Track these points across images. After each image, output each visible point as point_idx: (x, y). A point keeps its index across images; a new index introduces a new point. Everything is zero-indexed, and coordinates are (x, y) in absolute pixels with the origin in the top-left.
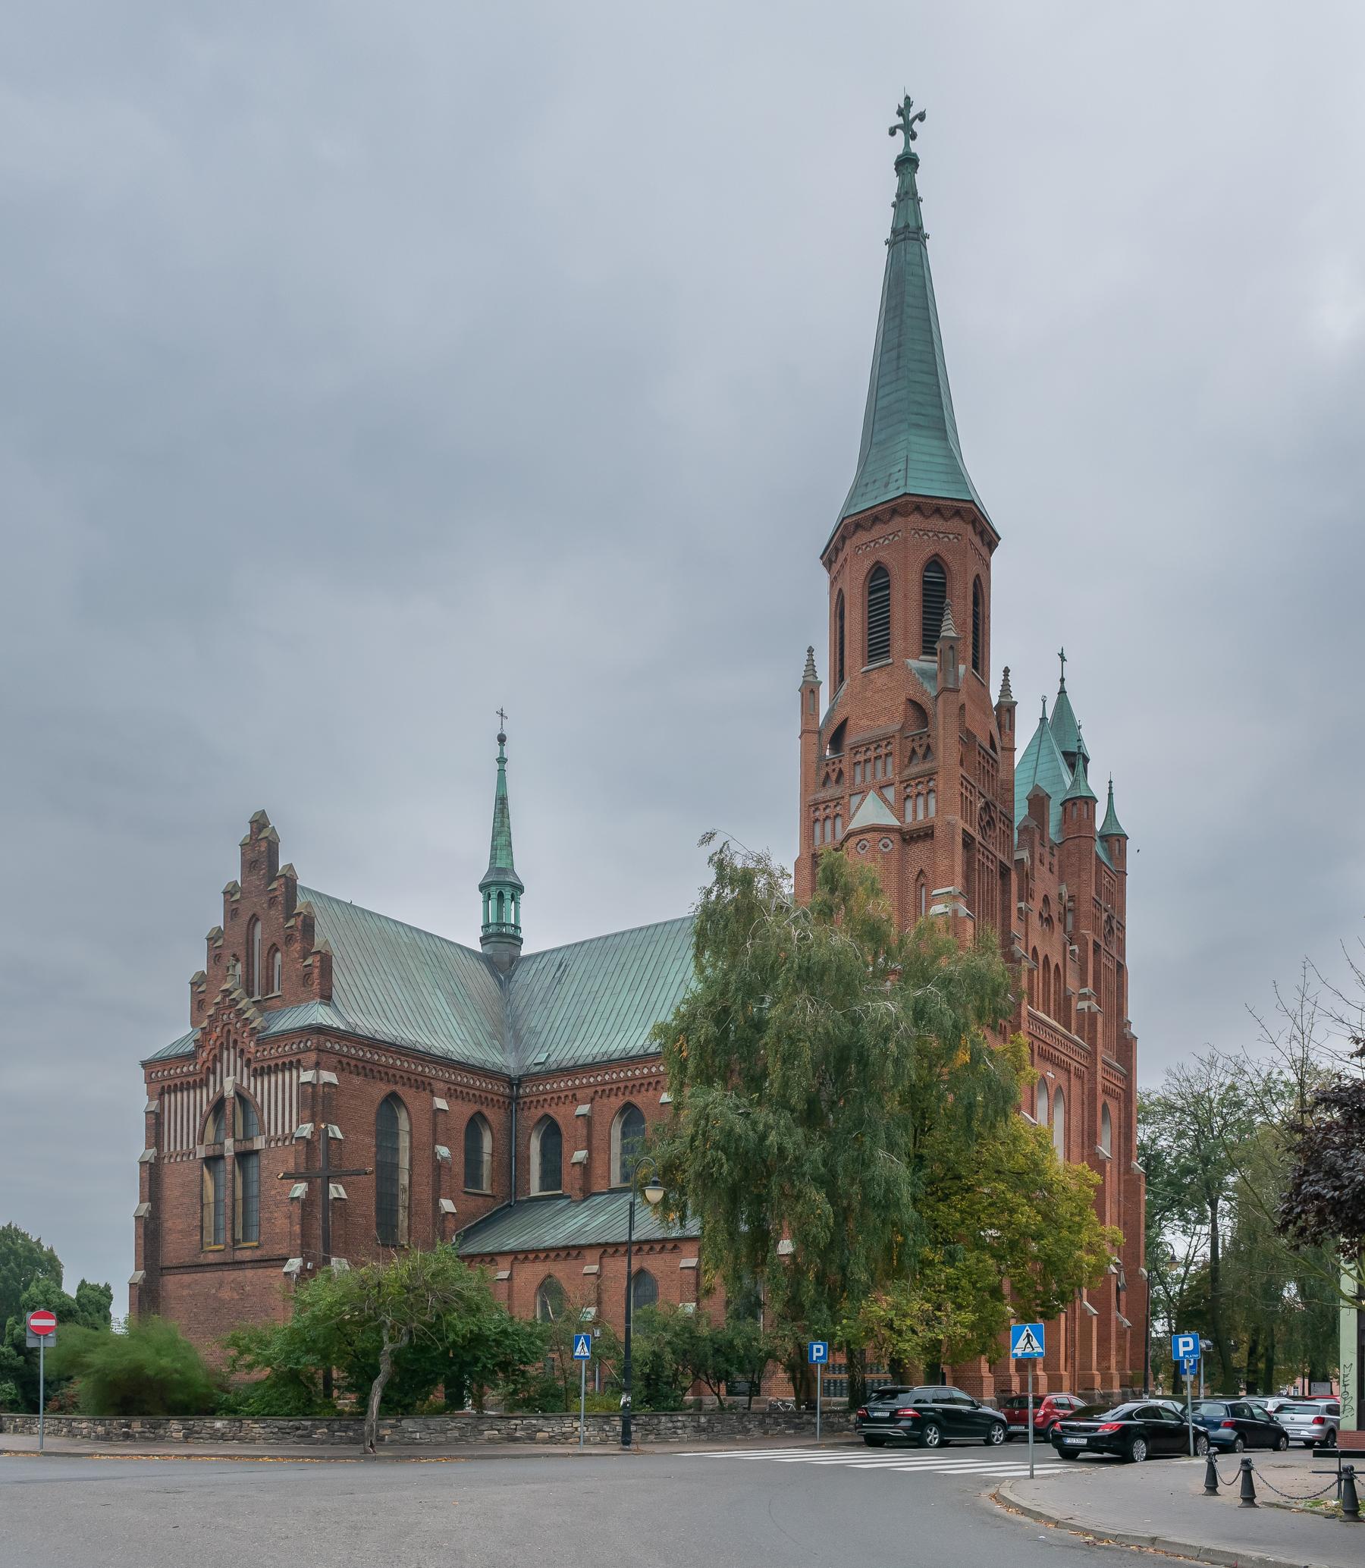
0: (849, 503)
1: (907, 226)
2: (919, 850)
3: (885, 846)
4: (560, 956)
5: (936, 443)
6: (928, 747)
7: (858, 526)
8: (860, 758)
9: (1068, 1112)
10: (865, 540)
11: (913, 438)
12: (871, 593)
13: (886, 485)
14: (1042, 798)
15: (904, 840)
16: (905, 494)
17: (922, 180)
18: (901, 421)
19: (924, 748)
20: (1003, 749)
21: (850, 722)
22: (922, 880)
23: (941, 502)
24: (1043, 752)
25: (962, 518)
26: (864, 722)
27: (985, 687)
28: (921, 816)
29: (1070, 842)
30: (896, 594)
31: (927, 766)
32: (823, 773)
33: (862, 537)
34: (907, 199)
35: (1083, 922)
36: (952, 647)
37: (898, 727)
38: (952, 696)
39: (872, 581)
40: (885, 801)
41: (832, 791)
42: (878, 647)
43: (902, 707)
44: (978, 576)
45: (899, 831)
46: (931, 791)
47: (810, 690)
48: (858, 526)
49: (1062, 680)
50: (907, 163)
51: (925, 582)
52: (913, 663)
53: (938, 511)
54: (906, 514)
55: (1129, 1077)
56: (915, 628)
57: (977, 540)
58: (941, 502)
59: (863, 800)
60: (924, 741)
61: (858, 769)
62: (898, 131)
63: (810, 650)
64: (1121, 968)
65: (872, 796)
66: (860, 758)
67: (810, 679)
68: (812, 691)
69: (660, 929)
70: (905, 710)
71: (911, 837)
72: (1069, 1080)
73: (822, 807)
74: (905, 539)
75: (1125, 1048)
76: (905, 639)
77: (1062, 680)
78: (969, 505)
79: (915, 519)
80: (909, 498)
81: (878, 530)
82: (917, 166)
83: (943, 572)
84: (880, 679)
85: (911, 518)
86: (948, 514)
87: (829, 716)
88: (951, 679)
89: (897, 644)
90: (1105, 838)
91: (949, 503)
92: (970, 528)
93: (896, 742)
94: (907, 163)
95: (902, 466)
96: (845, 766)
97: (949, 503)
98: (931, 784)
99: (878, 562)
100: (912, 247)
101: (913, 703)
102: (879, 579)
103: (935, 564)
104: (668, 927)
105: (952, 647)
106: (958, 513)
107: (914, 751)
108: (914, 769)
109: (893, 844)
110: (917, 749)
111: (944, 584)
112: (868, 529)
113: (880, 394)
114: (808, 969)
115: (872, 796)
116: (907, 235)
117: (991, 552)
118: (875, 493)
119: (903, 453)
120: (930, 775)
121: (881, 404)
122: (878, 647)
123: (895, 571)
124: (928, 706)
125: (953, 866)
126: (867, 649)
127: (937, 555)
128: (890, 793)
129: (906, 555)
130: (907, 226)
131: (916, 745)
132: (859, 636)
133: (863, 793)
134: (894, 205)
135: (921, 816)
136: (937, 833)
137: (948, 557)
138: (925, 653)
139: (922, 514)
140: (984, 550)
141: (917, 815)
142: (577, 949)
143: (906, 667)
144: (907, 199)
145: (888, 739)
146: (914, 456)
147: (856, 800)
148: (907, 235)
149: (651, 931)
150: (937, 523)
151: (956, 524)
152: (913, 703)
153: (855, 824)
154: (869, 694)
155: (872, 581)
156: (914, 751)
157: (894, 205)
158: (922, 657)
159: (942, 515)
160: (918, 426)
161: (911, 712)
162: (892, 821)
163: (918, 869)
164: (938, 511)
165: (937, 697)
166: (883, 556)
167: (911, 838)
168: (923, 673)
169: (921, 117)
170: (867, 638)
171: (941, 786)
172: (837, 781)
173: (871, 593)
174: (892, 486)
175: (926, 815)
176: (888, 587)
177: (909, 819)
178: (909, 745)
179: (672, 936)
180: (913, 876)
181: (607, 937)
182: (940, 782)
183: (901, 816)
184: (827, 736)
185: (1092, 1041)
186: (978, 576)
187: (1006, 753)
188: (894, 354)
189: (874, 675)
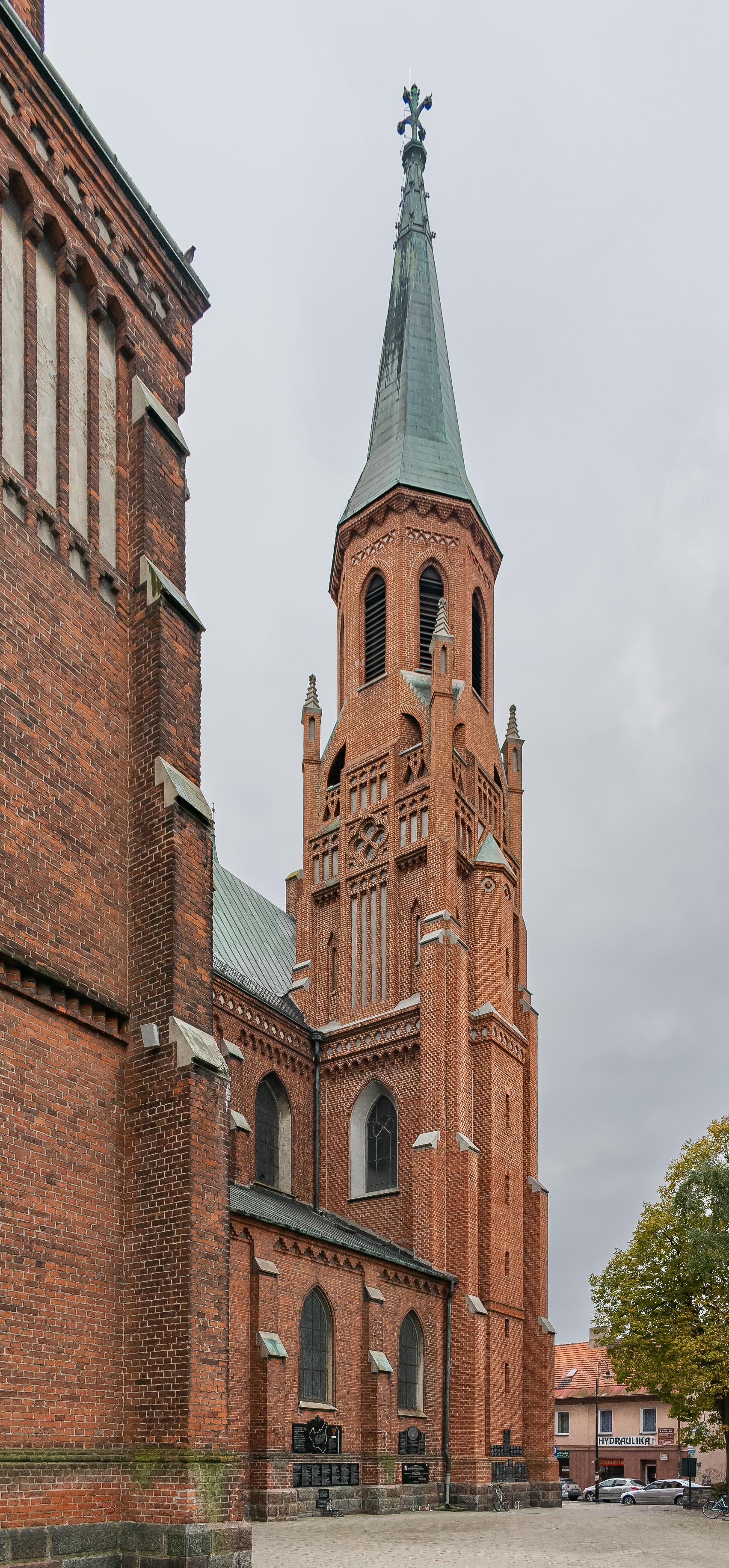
2: (414, 877)
8: (356, 890)
28: (414, 839)
30: (391, 600)
31: (423, 781)
33: (358, 544)
42: (375, 667)
44: (478, 589)
47: (311, 719)
48: (354, 533)
63: (312, 679)
66: (356, 890)
67: (311, 706)
68: (312, 719)
82: (424, 160)
92: (468, 534)
93: (391, 760)
94: (414, 154)
96: (343, 798)
99: (374, 569)
102: (375, 590)
106: (454, 515)
108: (413, 787)
116: (413, 233)
122: (375, 667)
129: (399, 561)
134: (403, 190)
135: (414, 839)
138: (421, 666)
148: (413, 233)
150: (431, 524)
151: (453, 528)
156: (410, 771)
157: (403, 190)
164: (434, 509)
169: (428, 104)
172: (337, 813)
184: (327, 767)
186: (478, 589)
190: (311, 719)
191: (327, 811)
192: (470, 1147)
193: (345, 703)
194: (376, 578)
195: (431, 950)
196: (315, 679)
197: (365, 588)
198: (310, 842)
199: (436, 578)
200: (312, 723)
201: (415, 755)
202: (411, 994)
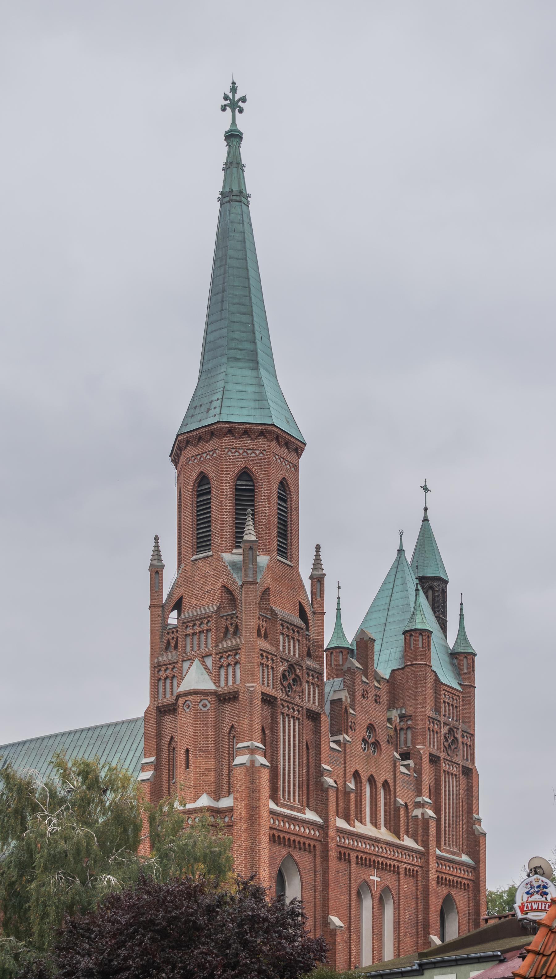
0: (183, 425)
1: (231, 191)
2: (229, 709)
3: (205, 706)
4: (6, 753)
5: (249, 373)
6: (237, 627)
7: (188, 442)
9: (397, 908)
10: (193, 453)
11: (231, 371)
12: (199, 496)
13: (208, 411)
14: (366, 642)
15: (220, 700)
16: (219, 422)
17: (247, 151)
18: (222, 355)
19: (234, 626)
20: (314, 613)
21: (184, 600)
22: (233, 733)
23: (248, 426)
24: (398, 582)
25: (266, 437)
26: (194, 601)
27: (294, 569)
28: (230, 683)
29: (408, 669)
32: (165, 640)
34: (234, 166)
35: (419, 739)
36: (251, 548)
37: (214, 608)
38: (251, 588)
39: (199, 486)
40: (206, 667)
41: (170, 656)
43: (219, 592)
45: (214, 693)
46: (236, 663)
47: (156, 571)
48: (188, 442)
49: (426, 509)
50: (233, 137)
51: (237, 490)
52: (227, 557)
53: (246, 433)
54: (221, 437)
55: (477, 869)
56: (229, 528)
57: (283, 451)
58: (248, 426)
59: (191, 666)
60: (234, 621)
61: (189, 639)
62: (228, 108)
64: (469, 773)
65: (197, 662)
66: (190, 631)
67: (155, 562)
68: (157, 573)
69: (84, 733)
70: (221, 594)
71: (227, 698)
72: (399, 880)
73: (163, 668)
74: (221, 456)
75: (474, 843)
76: (221, 537)
77: (426, 509)
78: (270, 428)
79: (228, 440)
80: (222, 425)
81: (202, 447)
82: (241, 138)
83: (252, 480)
84: (204, 567)
85: (225, 439)
86: (254, 435)
87: (170, 596)
88: (250, 574)
89: (216, 541)
90: (454, 655)
91: (254, 427)
92: (274, 444)
95: (219, 395)
97: (254, 427)
98: (237, 657)
100: (236, 208)
101: (225, 588)
103: (245, 474)
104: (90, 733)
105: (251, 548)
106: (262, 434)
107: (227, 628)
109: (210, 704)
110: (229, 626)
111: (253, 491)
112: (196, 445)
113: (210, 330)
114: (54, 856)
115: (197, 662)
116: (234, 197)
117: (299, 455)
118: (199, 417)
119: (221, 384)
120: (236, 650)
121: (210, 338)
123: (214, 482)
124: (236, 592)
125: (251, 725)
126: (195, 541)
127: (246, 468)
128: (209, 662)
129: (223, 465)
130: (231, 191)
131: (229, 623)
132: (190, 530)
133: (191, 660)
135: (230, 683)
136: (241, 697)
137: (255, 469)
139: (234, 436)
140: (291, 457)
141: (228, 683)
142: (20, 748)
143: (221, 559)
144: (234, 166)
145: (208, 617)
146: (229, 387)
147: (186, 665)
148: (234, 197)
149: (78, 735)
150: (246, 442)
152: (225, 588)
153: (184, 687)
154: (196, 579)
155: (199, 486)
156: (227, 628)
158: (235, 551)
159: (250, 436)
160: (235, 359)
161: (225, 596)
162: (211, 686)
163: (230, 724)
164: (246, 433)
165: (242, 586)
166: (207, 468)
167: (224, 699)
168: (234, 565)
170: (195, 532)
171: (243, 659)
173: (199, 496)
174: (212, 412)
175: (234, 682)
176: (209, 493)
177: (223, 683)
178: (223, 623)
179: (93, 742)
180: (226, 729)
181: (43, 739)
182: (242, 656)
183: (217, 681)
185: (425, 844)
187: (317, 616)
188: (219, 297)
189: (200, 564)
190: (156, 571)
191: (169, 643)
192: (357, 667)
193: (182, 566)
194: (203, 480)
195: (240, 770)
196: (320, 548)
197: (197, 482)
198: (183, 623)
199: (53, 739)
200: (157, 576)
201: (232, 618)
202: (229, 795)
